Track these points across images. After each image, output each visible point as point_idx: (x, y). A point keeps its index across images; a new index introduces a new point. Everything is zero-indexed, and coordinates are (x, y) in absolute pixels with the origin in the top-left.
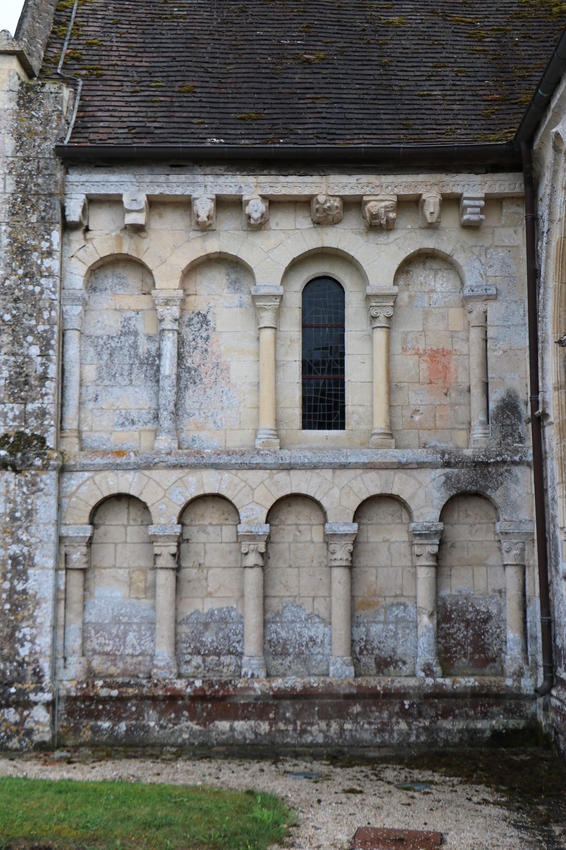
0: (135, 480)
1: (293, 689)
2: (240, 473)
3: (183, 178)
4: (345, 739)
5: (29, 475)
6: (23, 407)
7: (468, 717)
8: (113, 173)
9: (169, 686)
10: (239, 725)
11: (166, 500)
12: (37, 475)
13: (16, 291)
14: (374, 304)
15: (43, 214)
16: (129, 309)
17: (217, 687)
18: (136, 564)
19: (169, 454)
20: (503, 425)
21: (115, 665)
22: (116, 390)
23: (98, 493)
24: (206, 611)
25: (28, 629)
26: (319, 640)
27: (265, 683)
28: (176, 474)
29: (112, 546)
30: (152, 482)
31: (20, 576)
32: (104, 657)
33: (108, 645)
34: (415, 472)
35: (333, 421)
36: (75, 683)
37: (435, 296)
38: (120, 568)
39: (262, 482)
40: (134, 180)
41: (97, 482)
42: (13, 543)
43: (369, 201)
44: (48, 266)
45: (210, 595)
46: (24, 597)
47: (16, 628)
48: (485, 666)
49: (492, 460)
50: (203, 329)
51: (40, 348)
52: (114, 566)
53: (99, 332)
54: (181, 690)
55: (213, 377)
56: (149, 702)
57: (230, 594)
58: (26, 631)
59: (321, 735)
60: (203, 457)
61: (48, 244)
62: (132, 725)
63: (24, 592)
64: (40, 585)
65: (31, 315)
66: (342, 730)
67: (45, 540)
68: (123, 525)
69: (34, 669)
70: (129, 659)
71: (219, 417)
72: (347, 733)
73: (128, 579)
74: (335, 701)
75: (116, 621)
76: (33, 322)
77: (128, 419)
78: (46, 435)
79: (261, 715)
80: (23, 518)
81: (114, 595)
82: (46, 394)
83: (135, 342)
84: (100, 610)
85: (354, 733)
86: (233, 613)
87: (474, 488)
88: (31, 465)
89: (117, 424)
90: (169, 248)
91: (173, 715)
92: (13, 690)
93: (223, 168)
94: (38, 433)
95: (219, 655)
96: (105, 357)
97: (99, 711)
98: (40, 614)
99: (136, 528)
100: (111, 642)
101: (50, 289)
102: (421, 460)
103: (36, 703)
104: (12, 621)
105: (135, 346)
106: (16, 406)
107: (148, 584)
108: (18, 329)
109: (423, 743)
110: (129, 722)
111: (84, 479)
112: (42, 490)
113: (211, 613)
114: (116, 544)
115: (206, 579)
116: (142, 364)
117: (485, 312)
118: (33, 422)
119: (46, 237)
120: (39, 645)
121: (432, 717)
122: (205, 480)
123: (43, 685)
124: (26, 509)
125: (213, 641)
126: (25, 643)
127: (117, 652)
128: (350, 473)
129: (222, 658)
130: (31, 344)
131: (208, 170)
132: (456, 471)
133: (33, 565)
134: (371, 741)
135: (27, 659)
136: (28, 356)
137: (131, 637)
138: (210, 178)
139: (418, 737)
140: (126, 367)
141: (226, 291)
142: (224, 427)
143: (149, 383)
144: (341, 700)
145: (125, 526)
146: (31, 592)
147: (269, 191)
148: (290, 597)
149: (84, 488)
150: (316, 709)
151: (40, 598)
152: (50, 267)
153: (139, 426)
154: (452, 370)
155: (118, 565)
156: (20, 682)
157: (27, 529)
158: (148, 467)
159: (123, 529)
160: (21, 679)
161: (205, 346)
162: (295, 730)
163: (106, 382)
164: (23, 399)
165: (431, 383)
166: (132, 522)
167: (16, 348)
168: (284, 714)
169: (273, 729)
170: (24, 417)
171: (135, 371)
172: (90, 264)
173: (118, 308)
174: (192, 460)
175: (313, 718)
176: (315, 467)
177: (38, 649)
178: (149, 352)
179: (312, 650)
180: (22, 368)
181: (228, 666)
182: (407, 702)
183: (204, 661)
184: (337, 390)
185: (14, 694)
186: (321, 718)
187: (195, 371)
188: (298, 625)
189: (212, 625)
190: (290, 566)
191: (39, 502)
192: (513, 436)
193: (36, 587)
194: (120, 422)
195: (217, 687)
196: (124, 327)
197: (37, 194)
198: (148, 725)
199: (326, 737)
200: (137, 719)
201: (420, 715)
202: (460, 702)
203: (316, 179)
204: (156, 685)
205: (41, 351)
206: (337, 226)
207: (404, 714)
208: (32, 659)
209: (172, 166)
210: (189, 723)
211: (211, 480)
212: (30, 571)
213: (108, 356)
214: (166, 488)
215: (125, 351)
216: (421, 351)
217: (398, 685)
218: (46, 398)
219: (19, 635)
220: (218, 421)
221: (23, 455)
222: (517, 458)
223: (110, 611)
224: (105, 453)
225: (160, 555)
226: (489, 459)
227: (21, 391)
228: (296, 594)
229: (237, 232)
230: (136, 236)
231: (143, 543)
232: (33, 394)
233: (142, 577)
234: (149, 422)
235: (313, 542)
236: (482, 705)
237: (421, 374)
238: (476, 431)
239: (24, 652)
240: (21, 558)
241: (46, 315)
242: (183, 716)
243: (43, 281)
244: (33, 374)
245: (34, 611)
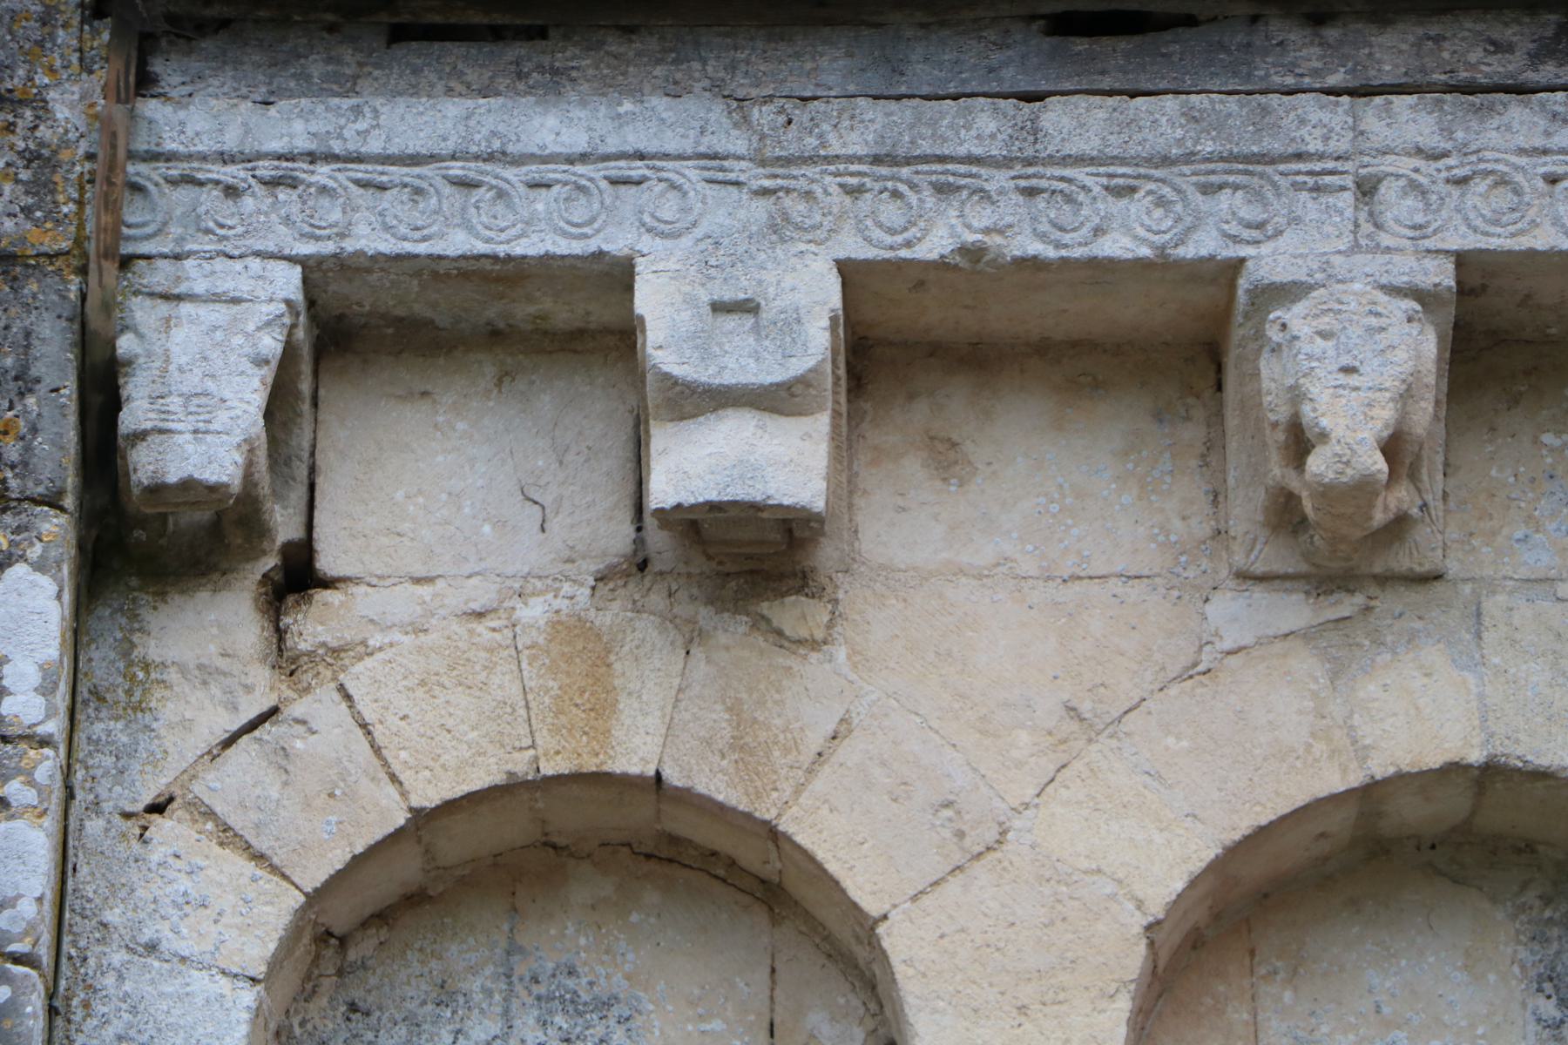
3: (1161, 120)
40: (738, 143)
138: (1407, 122)
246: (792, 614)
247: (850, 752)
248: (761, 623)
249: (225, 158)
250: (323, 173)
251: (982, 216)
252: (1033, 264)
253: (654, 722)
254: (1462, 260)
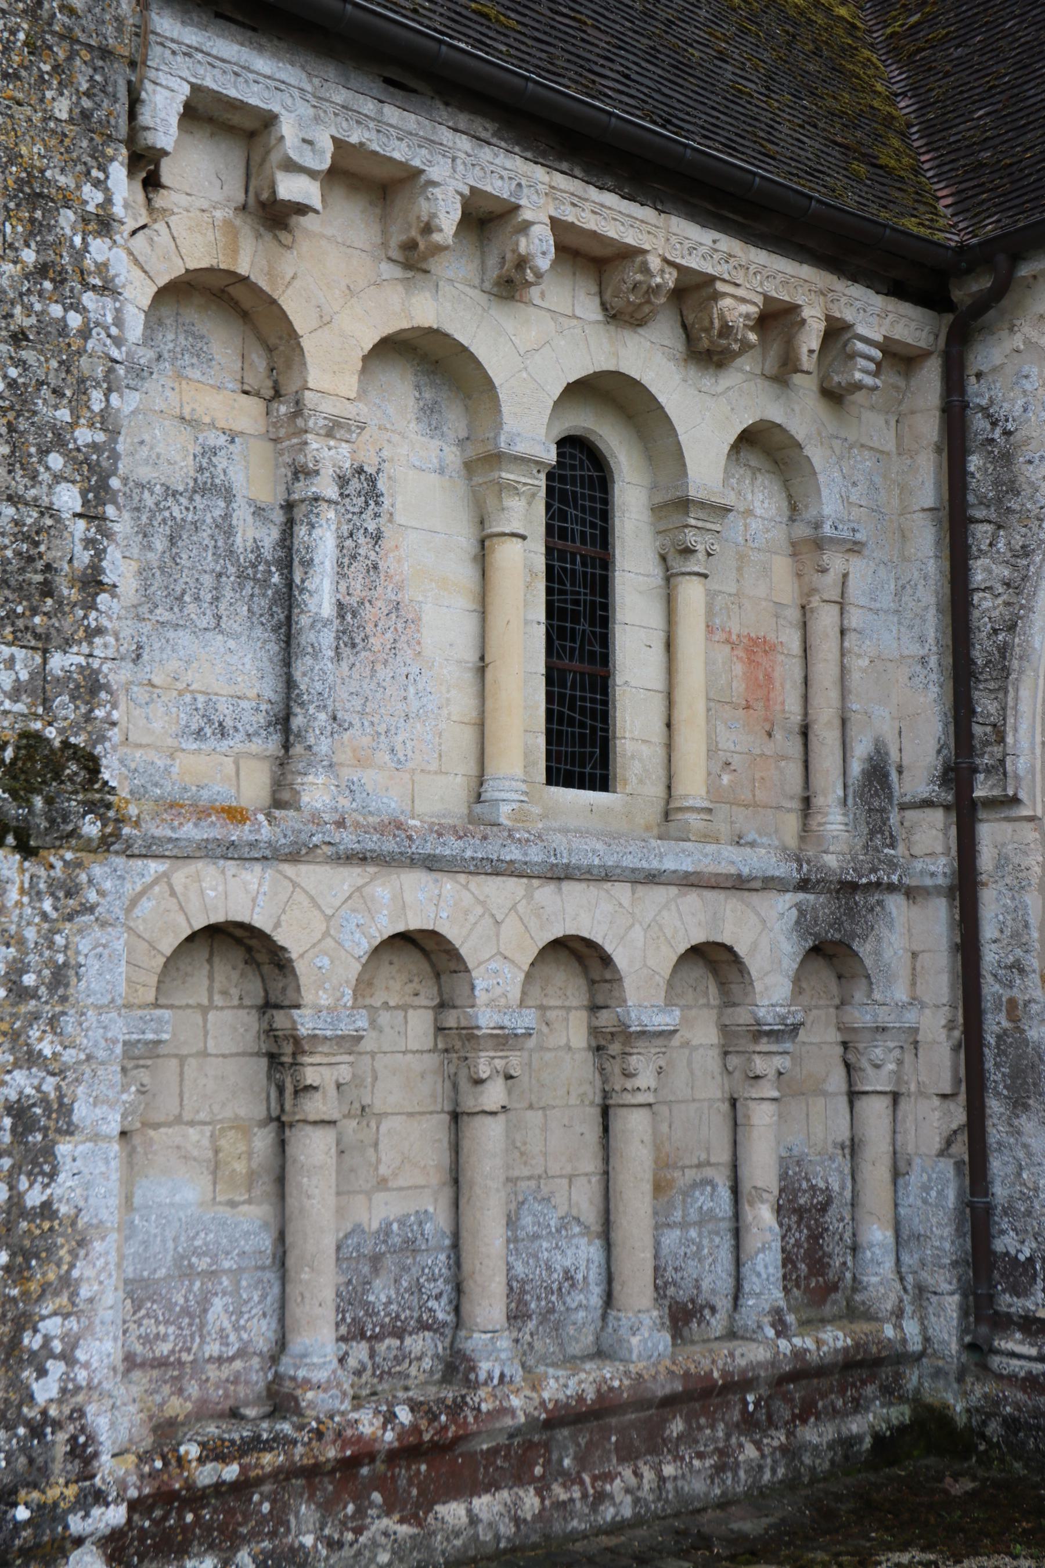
0: (265, 888)
1: (580, 1399)
2: (475, 882)
3: (411, 121)
4: (667, 1501)
5: (59, 865)
6: (38, 660)
7: (835, 1413)
8: (260, 49)
9: (349, 1432)
10: (484, 1504)
11: (329, 942)
12: (79, 864)
13: (18, 310)
14: (693, 522)
15: (86, 103)
16: (213, 425)
17: (443, 1418)
18: (228, 1113)
19: (341, 824)
20: (870, 810)
21: (180, 1391)
22: (183, 638)
23: (181, 919)
24: (375, 1226)
25: (58, 1320)
26: (579, 1277)
27: (528, 1393)
28: (351, 877)
29: (174, 1062)
30: (300, 897)
31: (35, 1163)
32: (155, 1373)
33: (165, 1338)
34: (755, 898)
35: (588, 770)
36: (132, 1458)
37: (754, 525)
38: (192, 1123)
39: (514, 907)
40: (309, 88)
41: (179, 889)
42: (16, 1065)
43: (725, 295)
44: (100, 259)
45: (382, 1184)
46: (46, 1225)
47: (25, 1322)
48: (822, 1301)
49: (864, 880)
50: (370, 512)
51: (84, 494)
52: (178, 1120)
53: (144, 473)
54: (374, 1439)
55: (389, 635)
56: (299, 1482)
57: (421, 1181)
58: (52, 1326)
59: (629, 1499)
60: (410, 838)
61: (99, 197)
62: (268, 1554)
63: (47, 1209)
64: (87, 1186)
65: (57, 392)
66: (662, 1479)
67: (101, 1054)
68: (199, 1006)
69: (74, 1438)
70: (212, 1372)
71: (400, 738)
72: (669, 1486)
73: (210, 1154)
74: (642, 1415)
75: (185, 1271)
76: (64, 415)
77: (210, 721)
78: (99, 750)
79: (520, 1477)
80: (43, 990)
81: (177, 1198)
82: (99, 631)
83: (227, 516)
84: (146, 1244)
85: (680, 1483)
86: (428, 1227)
87: (838, 936)
88: (73, 833)
89: (184, 732)
90: (339, 293)
91: (350, 1508)
92: (22, 1513)
93: (492, 126)
94: (78, 740)
95: (399, 1334)
96: (160, 544)
97: (185, 1528)
98: (89, 1272)
99: (228, 1015)
100: (171, 1329)
101: (106, 329)
102: (769, 873)
103: (79, 1542)
104: (14, 1300)
105: (226, 527)
106: (20, 654)
107: (254, 1165)
108: (23, 425)
109: (781, 1482)
110: (257, 1548)
111: (148, 879)
112: (91, 909)
113: (386, 1231)
114: (182, 1059)
115: (376, 1145)
116: (241, 576)
117: (845, 576)
118: (66, 708)
119: (95, 173)
120: (86, 1365)
121: (787, 1423)
122: (408, 897)
123: (98, 1481)
124: (50, 962)
125: (390, 1302)
126: (50, 1364)
127: (185, 1357)
128: (660, 894)
129: (408, 1341)
130: (58, 478)
131: (463, 120)
132: (811, 897)
133: (69, 1131)
134: (707, 1494)
135: (53, 1412)
136: (48, 510)
137: (218, 1309)
138: (464, 143)
139: (774, 1471)
140: (208, 580)
141: (413, 425)
142: (410, 765)
143: (258, 632)
144: (653, 1411)
145: (204, 1010)
146: (63, 1209)
147: (570, 215)
148: (529, 1178)
149: (146, 905)
150: (614, 1439)
151: (89, 1225)
152: (105, 265)
153: (236, 743)
154: (777, 684)
155: (187, 1116)
156: (35, 1486)
157: (53, 1022)
158: (294, 857)
159: (198, 1018)
160: (37, 1475)
161: (372, 555)
162: (585, 1496)
163: (162, 614)
164: (37, 636)
165: (747, 707)
166: (218, 1000)
167: (19, 483)
168: (560, 1461)
169: (547, 1502)
170: (40, 689)
171: (228, 594)
172: (162, 281)
173: (187, 412)
174: (390, 845)
175: (609, 1460)
176: (605, 876)
177: (82, 1376)
178: (257, 548)
179: (568, 1299)
180: (37, 544)
181: (419, 1359)
182: (750, 1398)
183: (372, 1355)
184: (593, 701)
185: (28, 1522)
186: (621, 1460)
187: (354, 616)
188: (545, 1245)
189: (389, 1261)
190: (531, 1107)
191: (84, 945)
192: (882, 833)
193: (76, 1195)
194: (194, 727)
195: (443, 1418)
196: (201, 469)
197: (67, 36)
198: (302, 1546)
199: (637, 1501)
200: (273, 1535)
201: (771, 1423)
202: (824, 1383)
203: (647, 213)
204: (319, 1434)
205: (86, 503)
206: (640, 330)
207: (749, 1424)
208: (67, 1411)
209: (388, 81)
210: (385, 1522)
211: (420, 896)
212: (63, 1148)
213: (167, 543)
214: (329, 912)
215: (205, 535)
216: (734, 637)
217: (743, 1363)
218: (97, 640)
219: (32, 1341)
220: (399, 747)
221: (49, 801)
222: (895, 878)
223: (170, 1244)
224: (202, 813)
225: (316, 1088)
226: (860, 877)
227: (34, 611)
228: (539, 1171)
229: (468, 290)
230: (268, 237)
231: (244, 1054)
232: (67, 624)
233: (242, 1147)
234: (257, 734)
235: (570, 1048)
236: (853, 1385)
237: (735, 684)
238: (831, 818)
239: (45, 1391)
240: (38, 1111)
241: (97, 399)
242: (372, 1505)
243: (88, 299)
244: (66, 567)
245: (72, 1266)
246: (284, 236)
247: (297, 283)
248: (276, 237)
249: (173, 40)
250: (199, 56)
251: (367, 135)
252: (375, 153)
253: (248, 259)
254: (473, 189)
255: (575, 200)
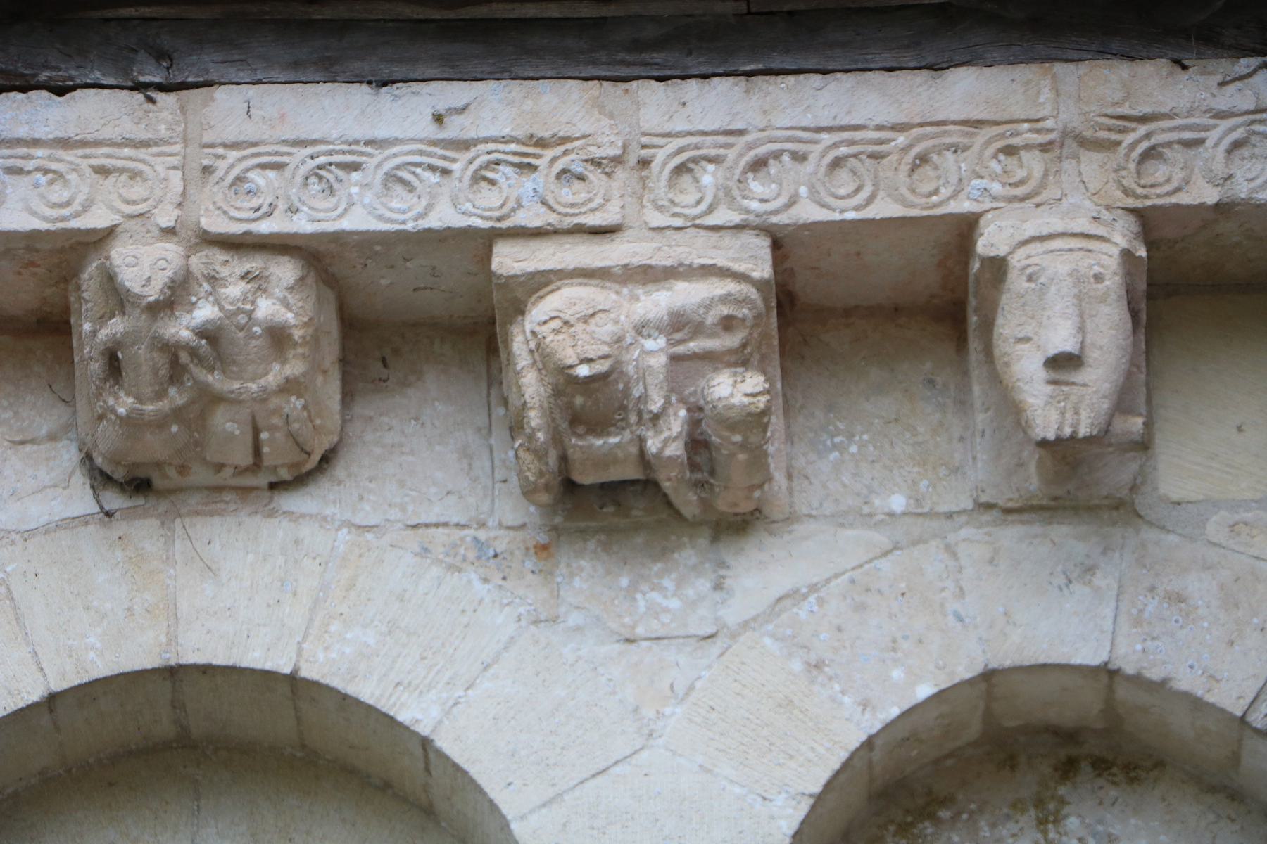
43: (541, 282)
255: (101, 156)
